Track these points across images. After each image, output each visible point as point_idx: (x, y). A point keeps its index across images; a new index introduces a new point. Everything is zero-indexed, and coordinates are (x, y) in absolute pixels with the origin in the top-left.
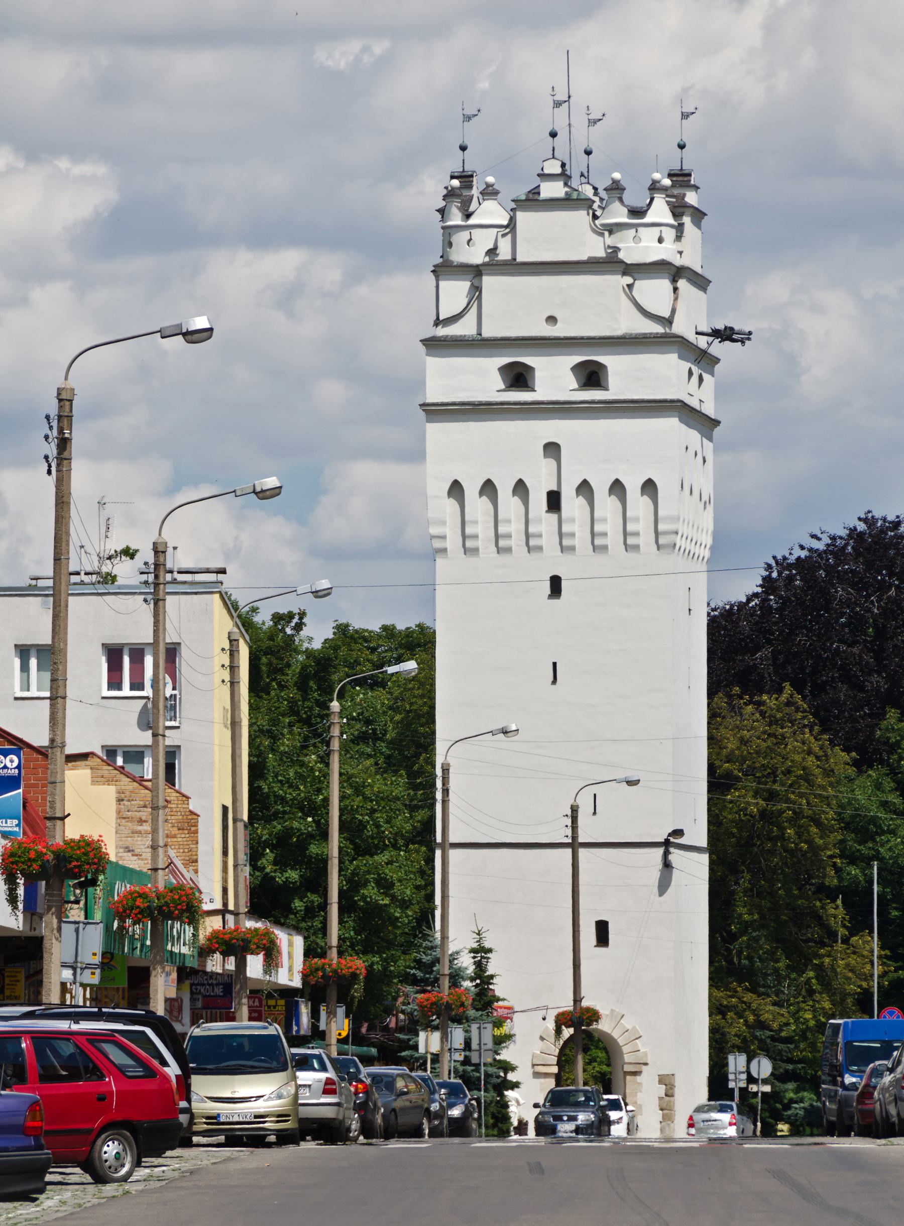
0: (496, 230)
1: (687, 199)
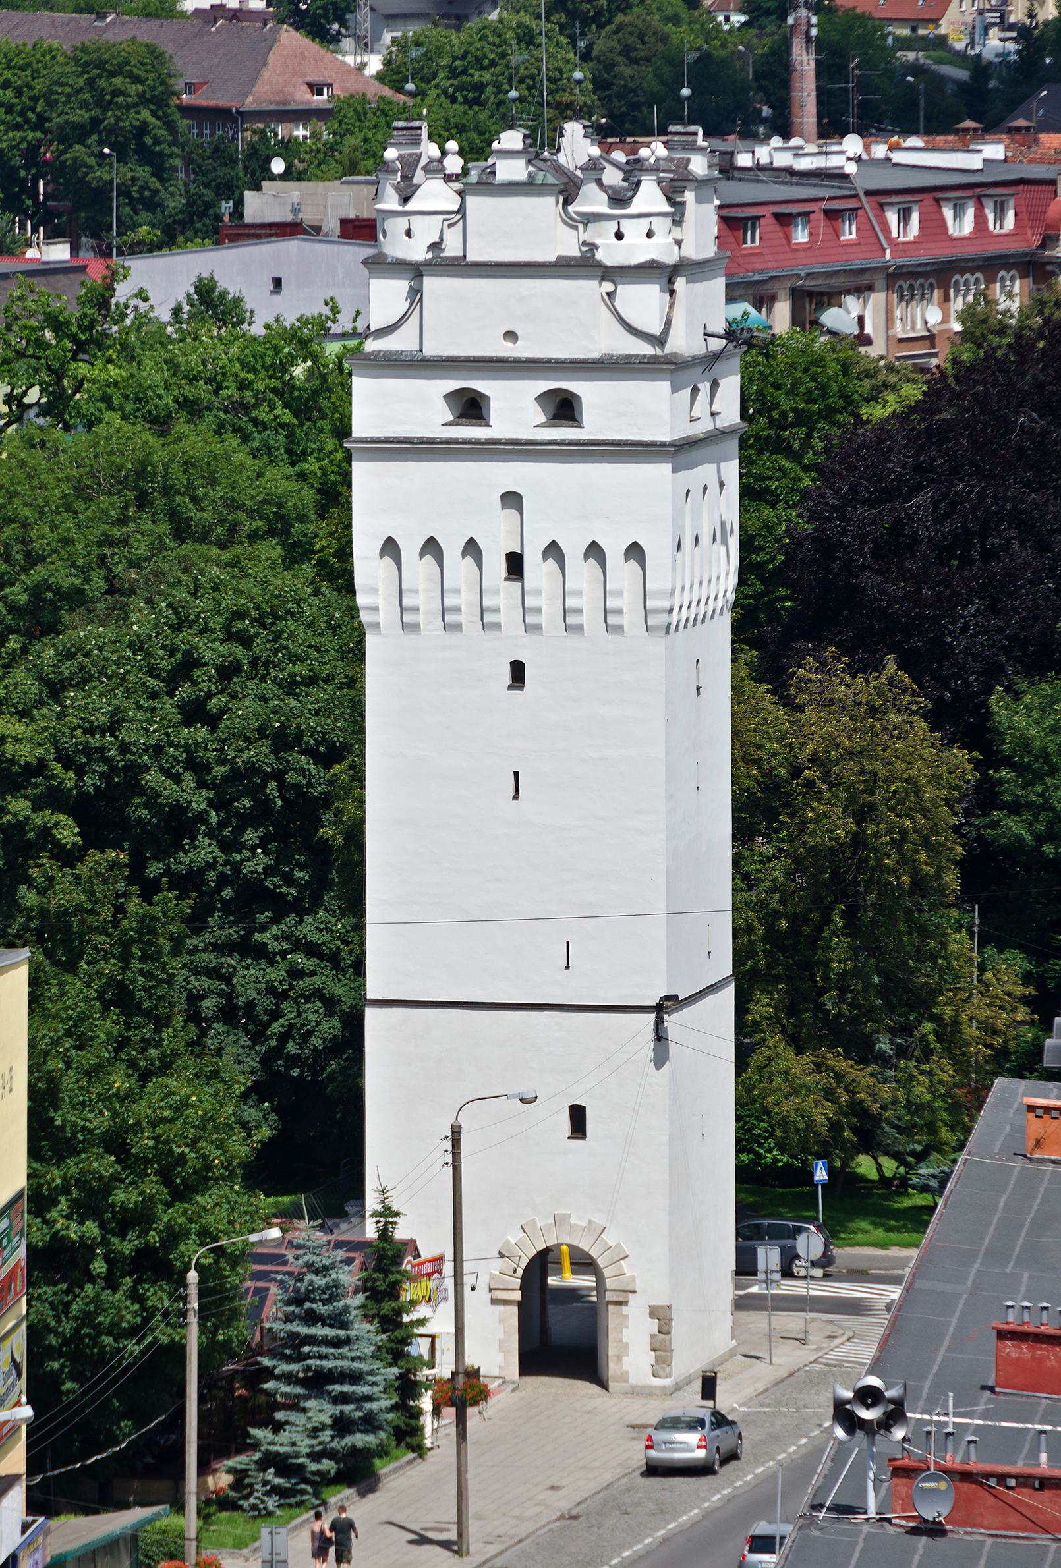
0: (441, 217)
1: (691, 167)
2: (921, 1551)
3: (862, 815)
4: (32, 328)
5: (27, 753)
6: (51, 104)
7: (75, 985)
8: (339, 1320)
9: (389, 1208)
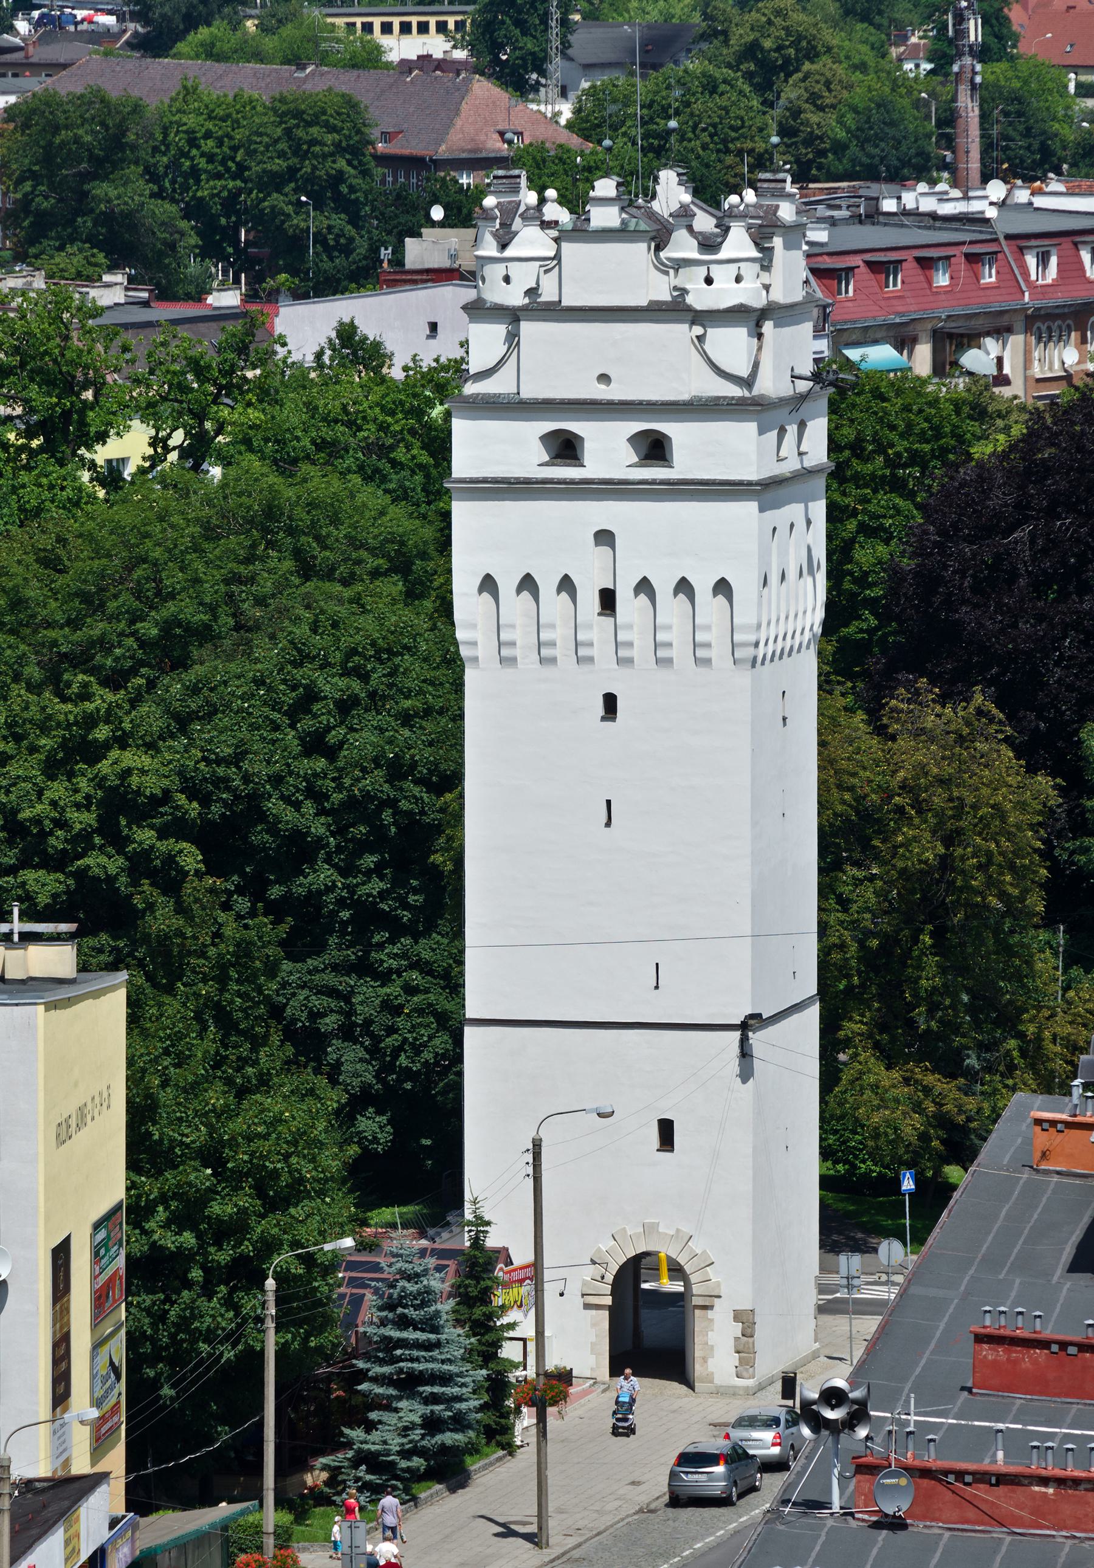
0: (538, 263)
2: (880, 1544)
3: (949, 841)
4: (174, 373)
5: (152, 785)
6: (251, 153)
7: (172, 1006)
8: (431, 1325)
9: (481, 1218)
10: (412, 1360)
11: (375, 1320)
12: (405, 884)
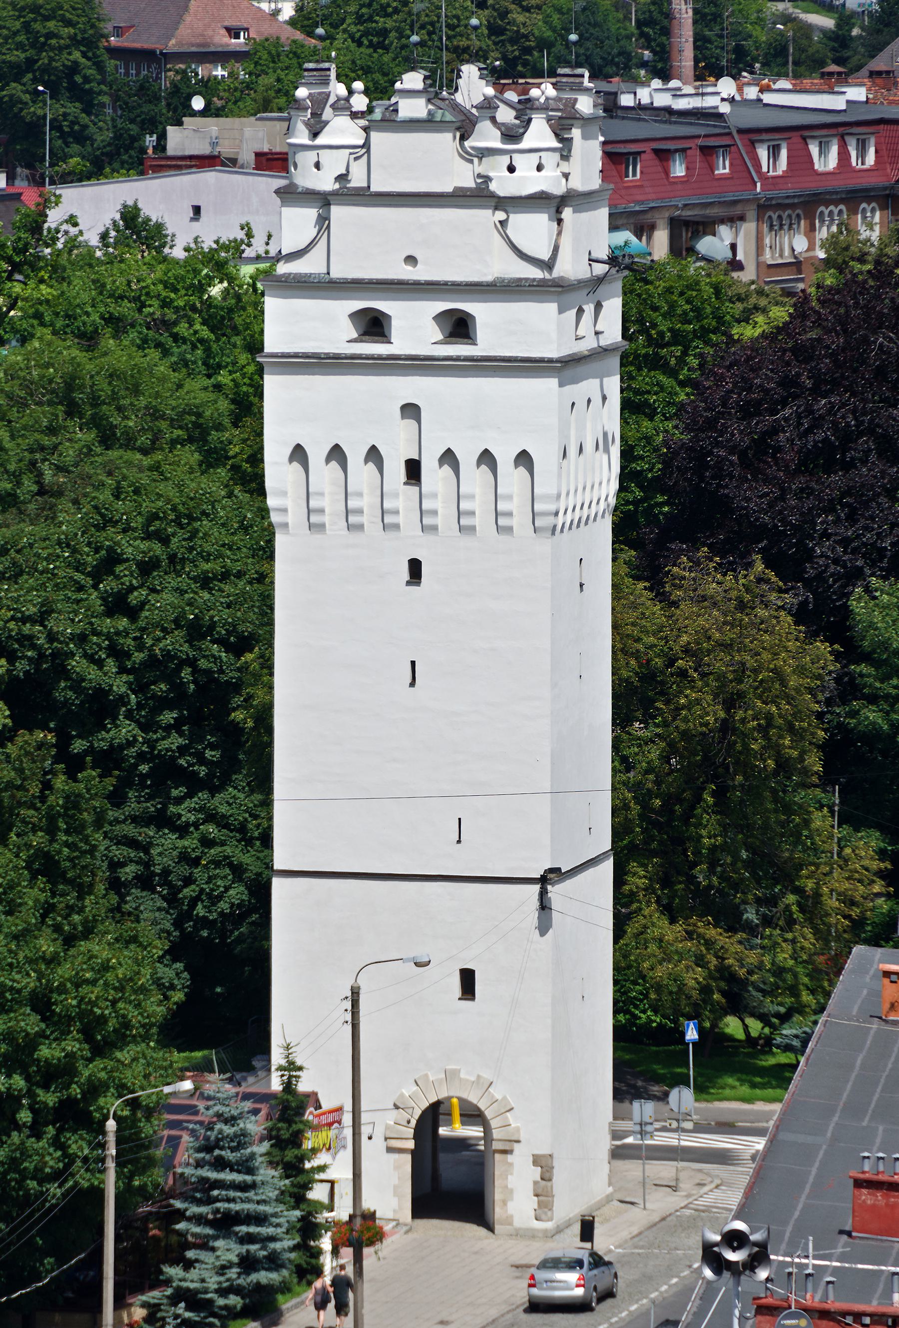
0: (348, 151)
10: (229, 1200)
11: (191, 1161)
12: (201, 740)
